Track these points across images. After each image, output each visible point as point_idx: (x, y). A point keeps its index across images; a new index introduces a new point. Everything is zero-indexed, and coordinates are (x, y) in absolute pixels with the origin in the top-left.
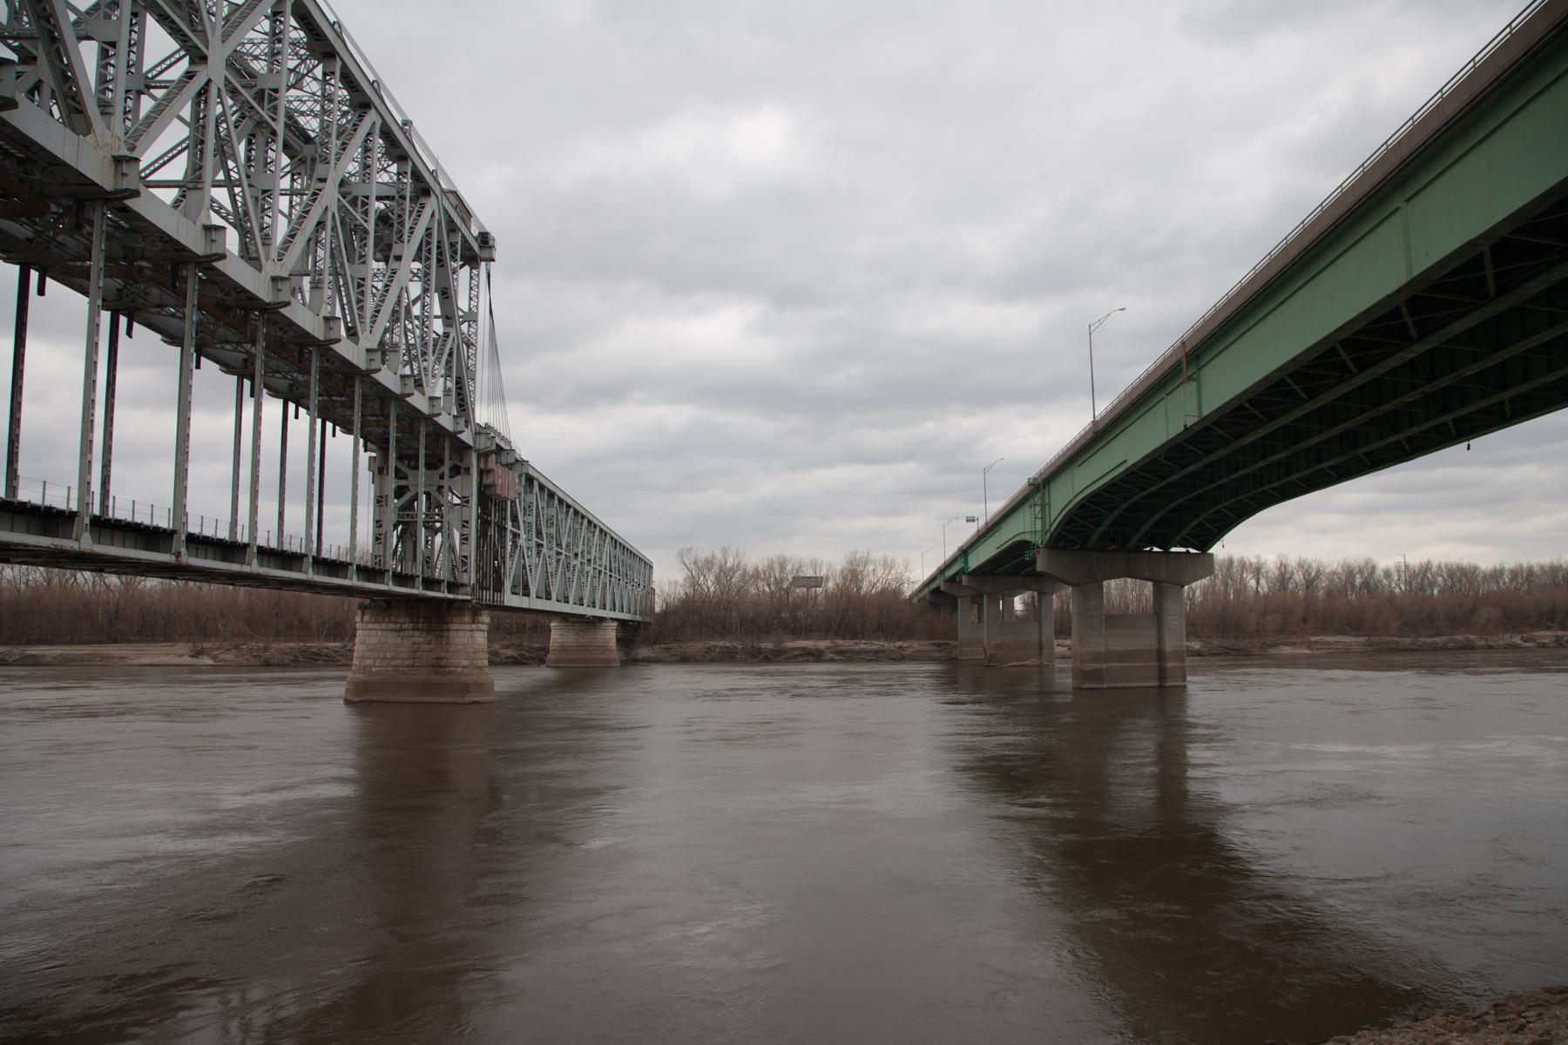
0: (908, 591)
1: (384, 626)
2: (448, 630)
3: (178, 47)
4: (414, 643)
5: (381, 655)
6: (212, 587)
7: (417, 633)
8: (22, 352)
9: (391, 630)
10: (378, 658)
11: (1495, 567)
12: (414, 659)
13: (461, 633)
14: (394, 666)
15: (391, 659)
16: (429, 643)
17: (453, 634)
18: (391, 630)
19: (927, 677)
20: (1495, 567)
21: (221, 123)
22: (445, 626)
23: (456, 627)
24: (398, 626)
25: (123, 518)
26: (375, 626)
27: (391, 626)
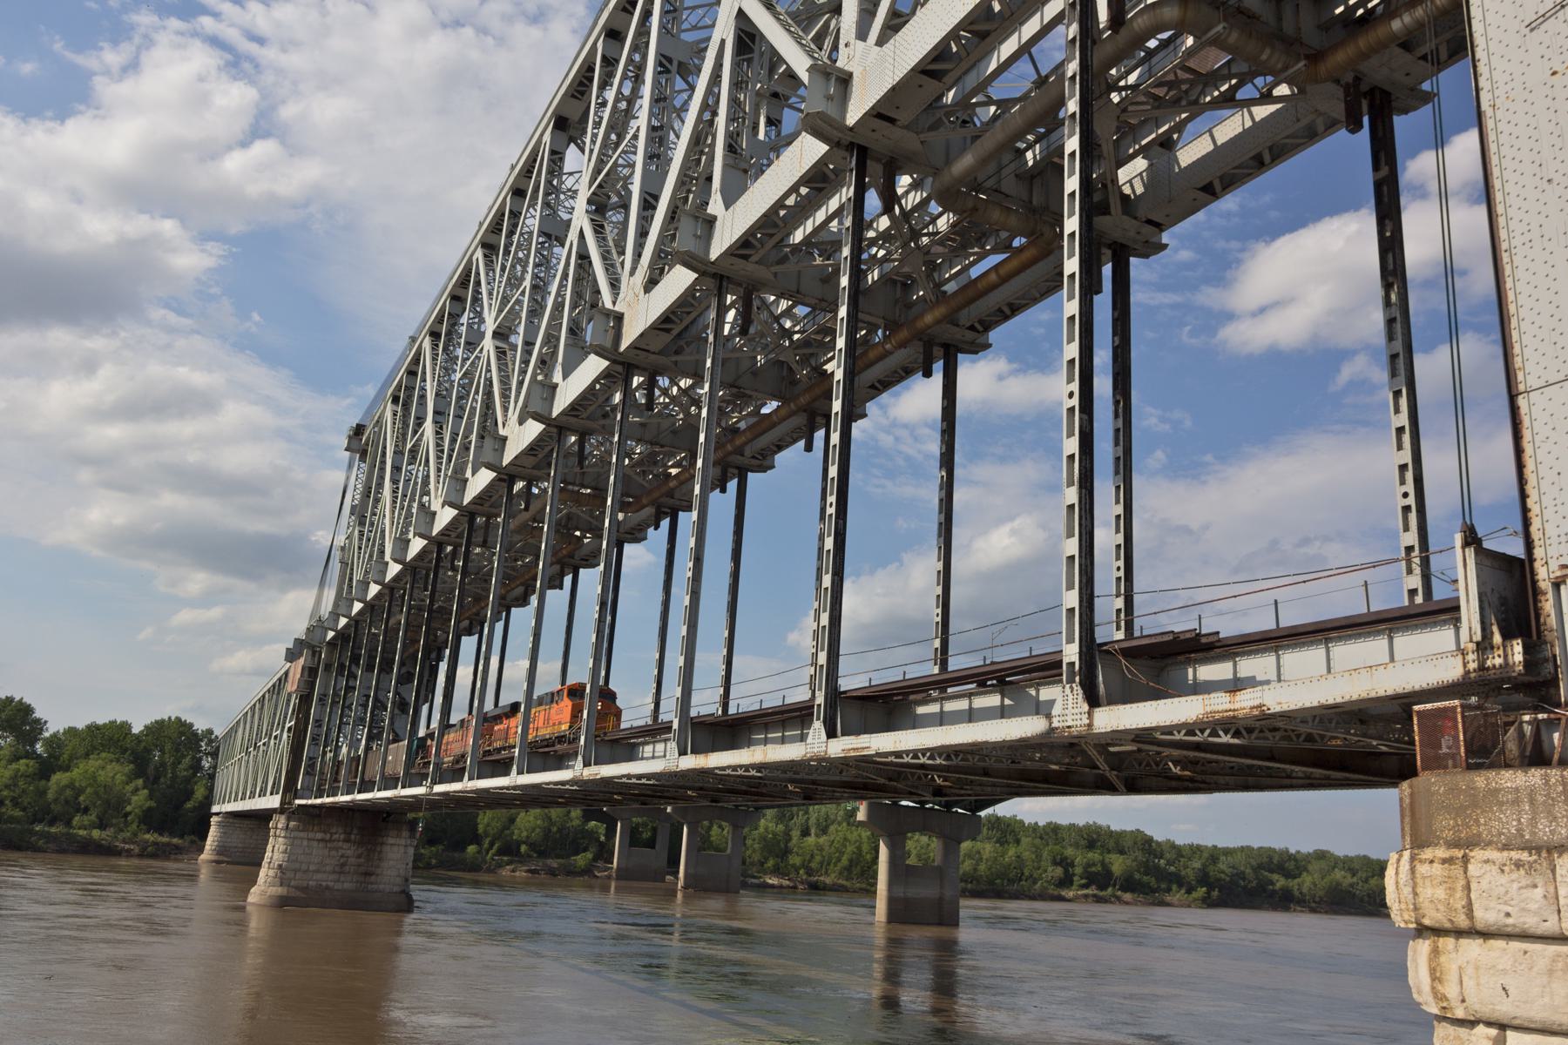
0: (136, 730)
1: (311, 835)
2: (382, 844)
3: (1250, 85)
4: (342, 856)
5: (304, 867)
6: (875, 965)
7: (346, 846)
8: (946, 402)
9: (318, 840)
10: (299, 870)
11: (1036, 823)
12: (340, 873)
13: (395, 849)
14: (317, 880)
15: (314, 871)
16: (359, 857)
17: (386, 848)
18: (318, 840)
19: (984, 969)
20: (1036, 823)
21: (782, 327)
22: (380, 840)
23: (391, 841)
24: (328, 836)
25: (1129, 827)
26: (302, 834)
27: (319, 836)
